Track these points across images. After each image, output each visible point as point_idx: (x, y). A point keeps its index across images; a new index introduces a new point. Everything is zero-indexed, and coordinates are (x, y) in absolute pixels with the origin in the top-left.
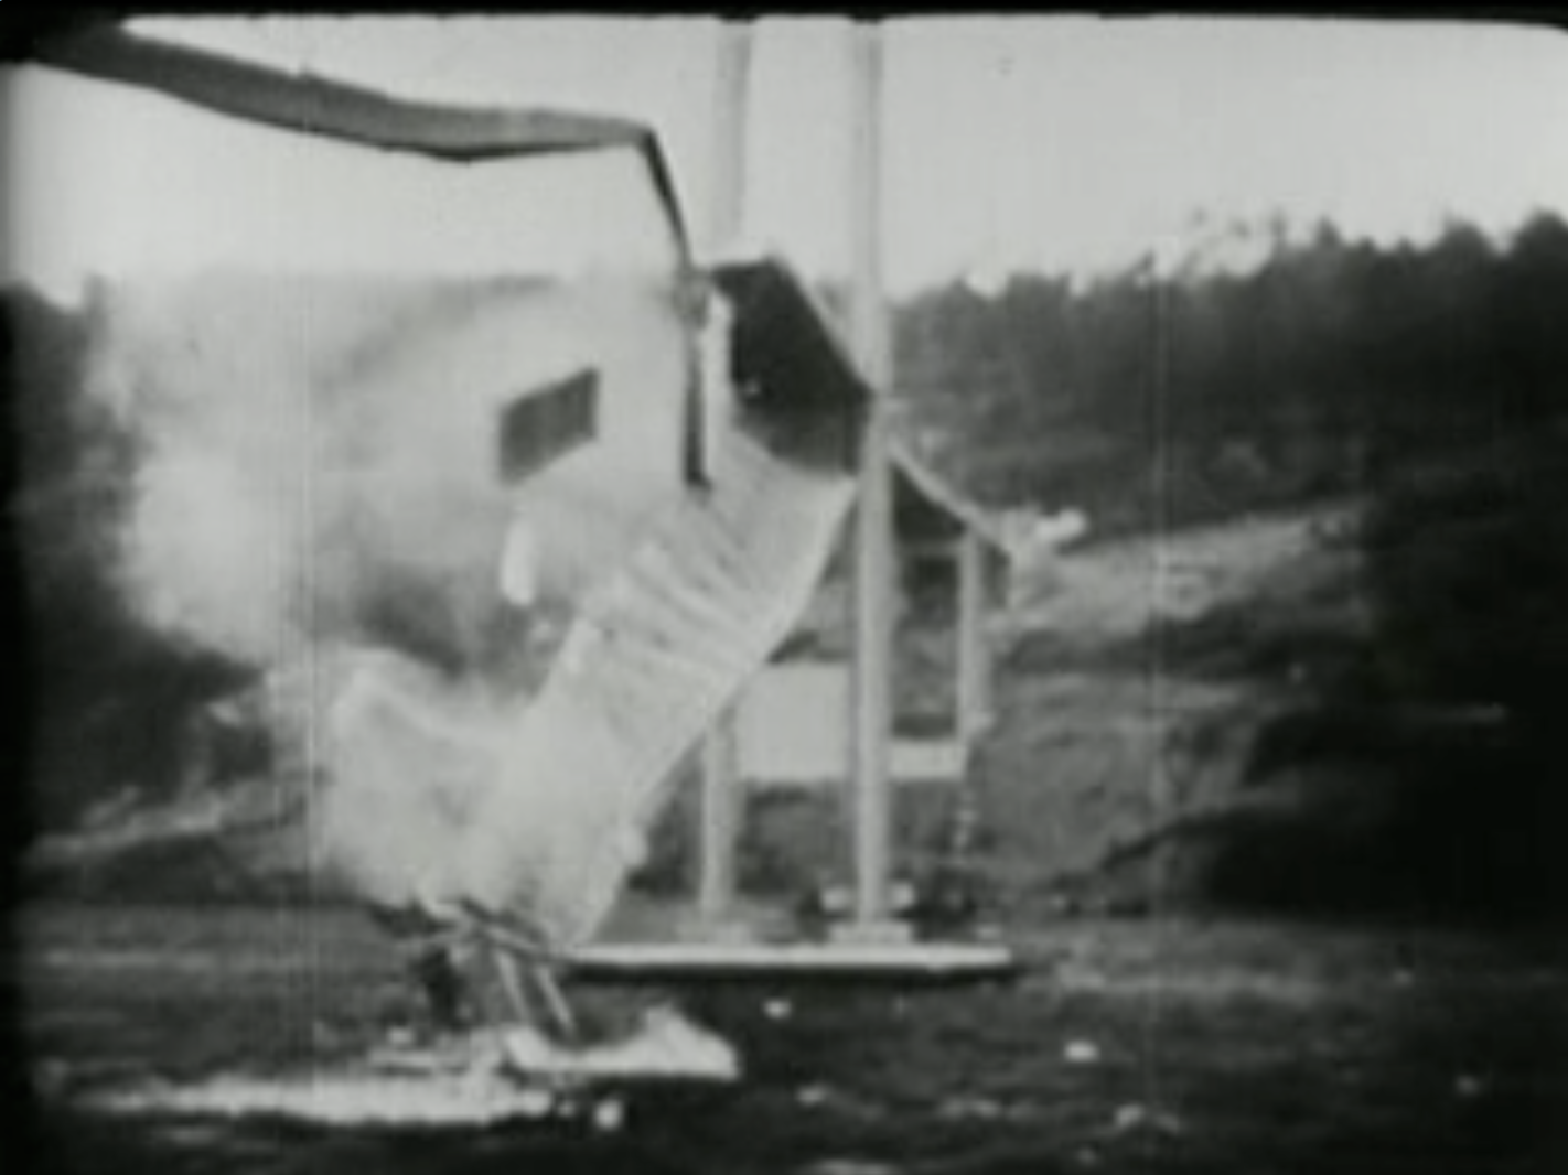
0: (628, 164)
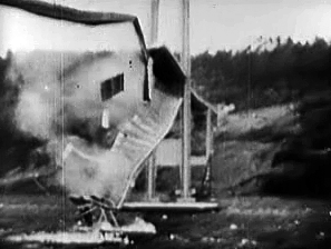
0: (130, 26)
